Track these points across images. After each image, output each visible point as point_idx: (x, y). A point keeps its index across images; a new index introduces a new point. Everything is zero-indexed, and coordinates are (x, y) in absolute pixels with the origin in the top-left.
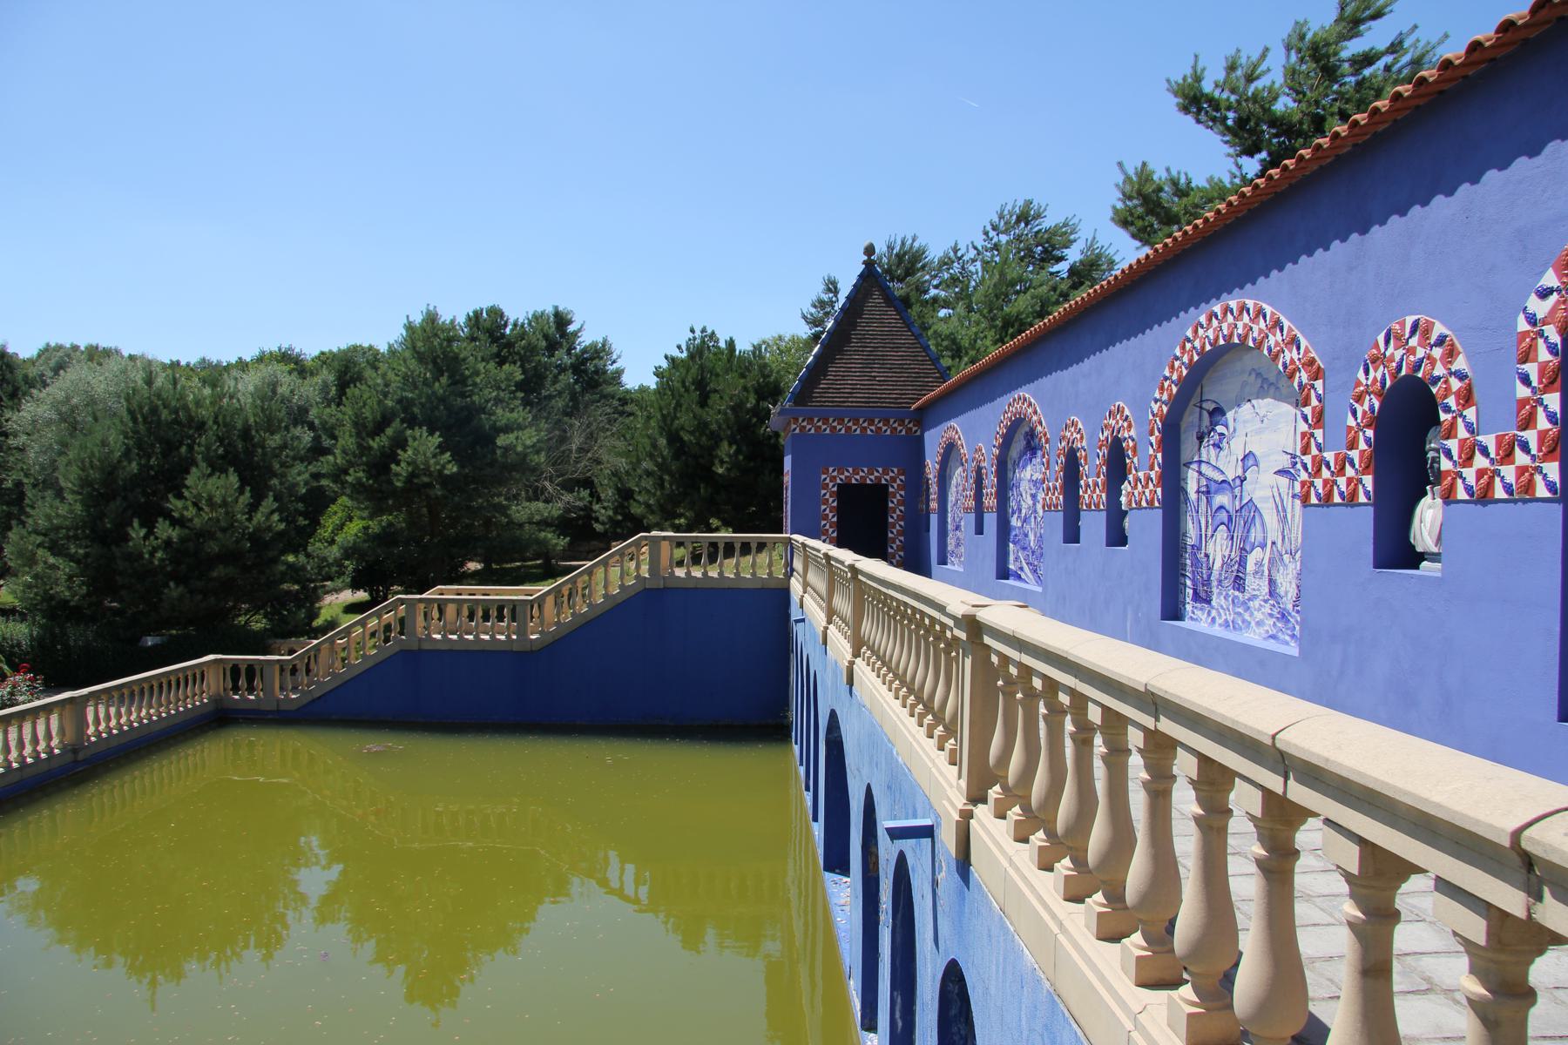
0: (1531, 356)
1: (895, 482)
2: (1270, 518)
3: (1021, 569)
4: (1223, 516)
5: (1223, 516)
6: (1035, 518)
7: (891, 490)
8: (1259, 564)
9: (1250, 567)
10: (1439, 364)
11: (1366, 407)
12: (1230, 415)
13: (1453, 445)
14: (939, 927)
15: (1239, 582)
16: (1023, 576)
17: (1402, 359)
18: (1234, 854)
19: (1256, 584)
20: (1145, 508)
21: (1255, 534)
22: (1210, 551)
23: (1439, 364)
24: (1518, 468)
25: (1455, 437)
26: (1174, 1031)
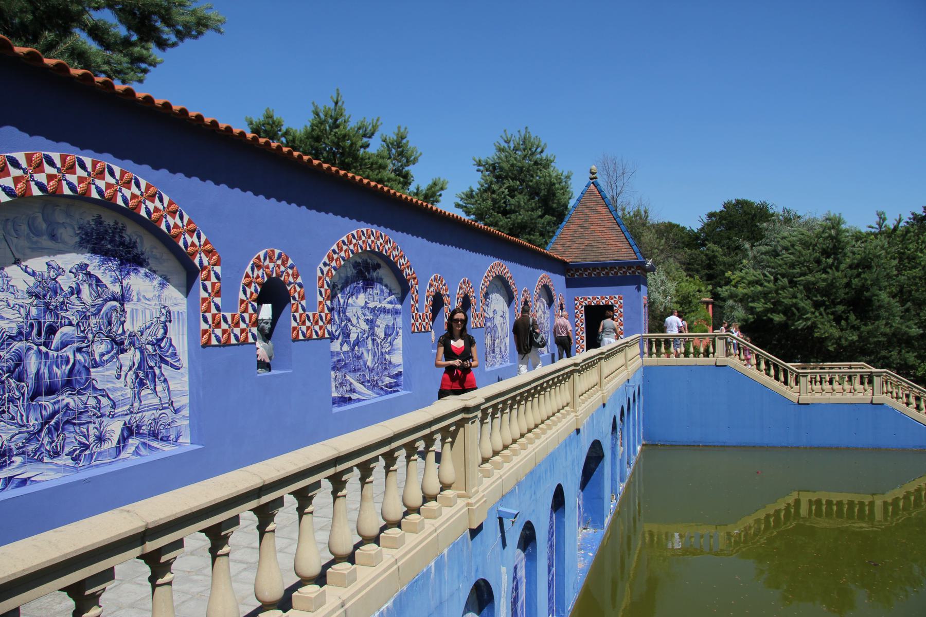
0: (208, 279)
1: (617, 303)
2: (499, 329)
3: (353, 391)
4: (489, 329)
5: (489, 329)
6: (373, 340)
7: (615, 308)
8: (498, 344)
9: (496, 345)
10: (291, 277)
11: (253, 289)
12: (490, 296)
13: (617, 314)
14: (498, 527)
15: (493, 352)
16: (354, 396)
17: (273, 268)
18: (278, 537)
19: (497, 350)
20: (314, 339)
21: (497, 335)
22: (486, 342)
23: (291, 277)
24: (241, 329)
25: (210, 312)
26: (431, 518)
